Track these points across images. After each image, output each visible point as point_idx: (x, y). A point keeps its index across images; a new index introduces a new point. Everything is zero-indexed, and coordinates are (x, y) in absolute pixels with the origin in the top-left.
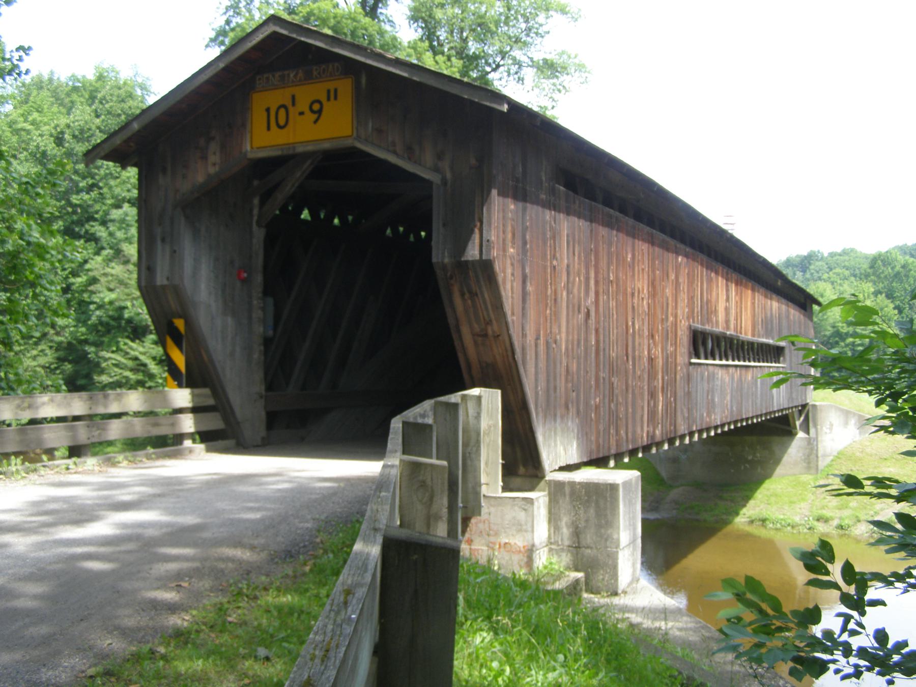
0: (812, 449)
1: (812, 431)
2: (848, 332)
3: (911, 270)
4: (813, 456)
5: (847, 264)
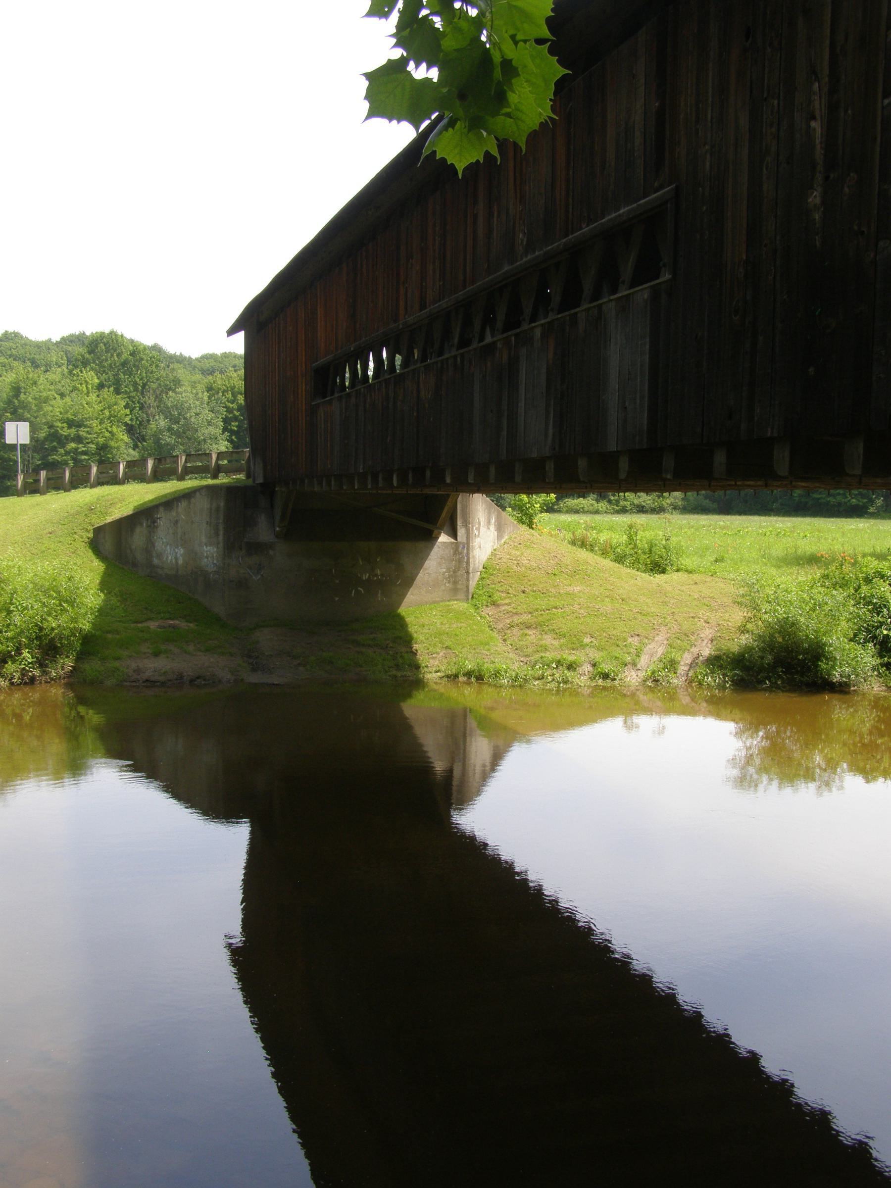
0: (460, 561)
1: (461, 532)
2: (69, 435)
3: (142, 359)
4: (462, 572)
5: (14, 352)
